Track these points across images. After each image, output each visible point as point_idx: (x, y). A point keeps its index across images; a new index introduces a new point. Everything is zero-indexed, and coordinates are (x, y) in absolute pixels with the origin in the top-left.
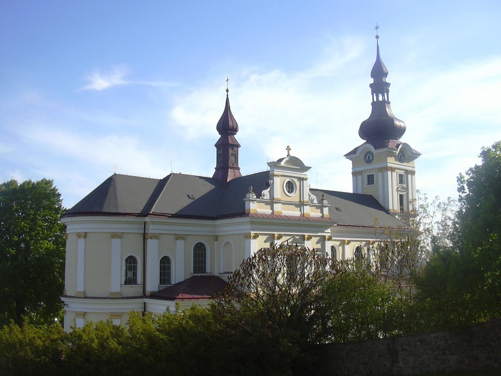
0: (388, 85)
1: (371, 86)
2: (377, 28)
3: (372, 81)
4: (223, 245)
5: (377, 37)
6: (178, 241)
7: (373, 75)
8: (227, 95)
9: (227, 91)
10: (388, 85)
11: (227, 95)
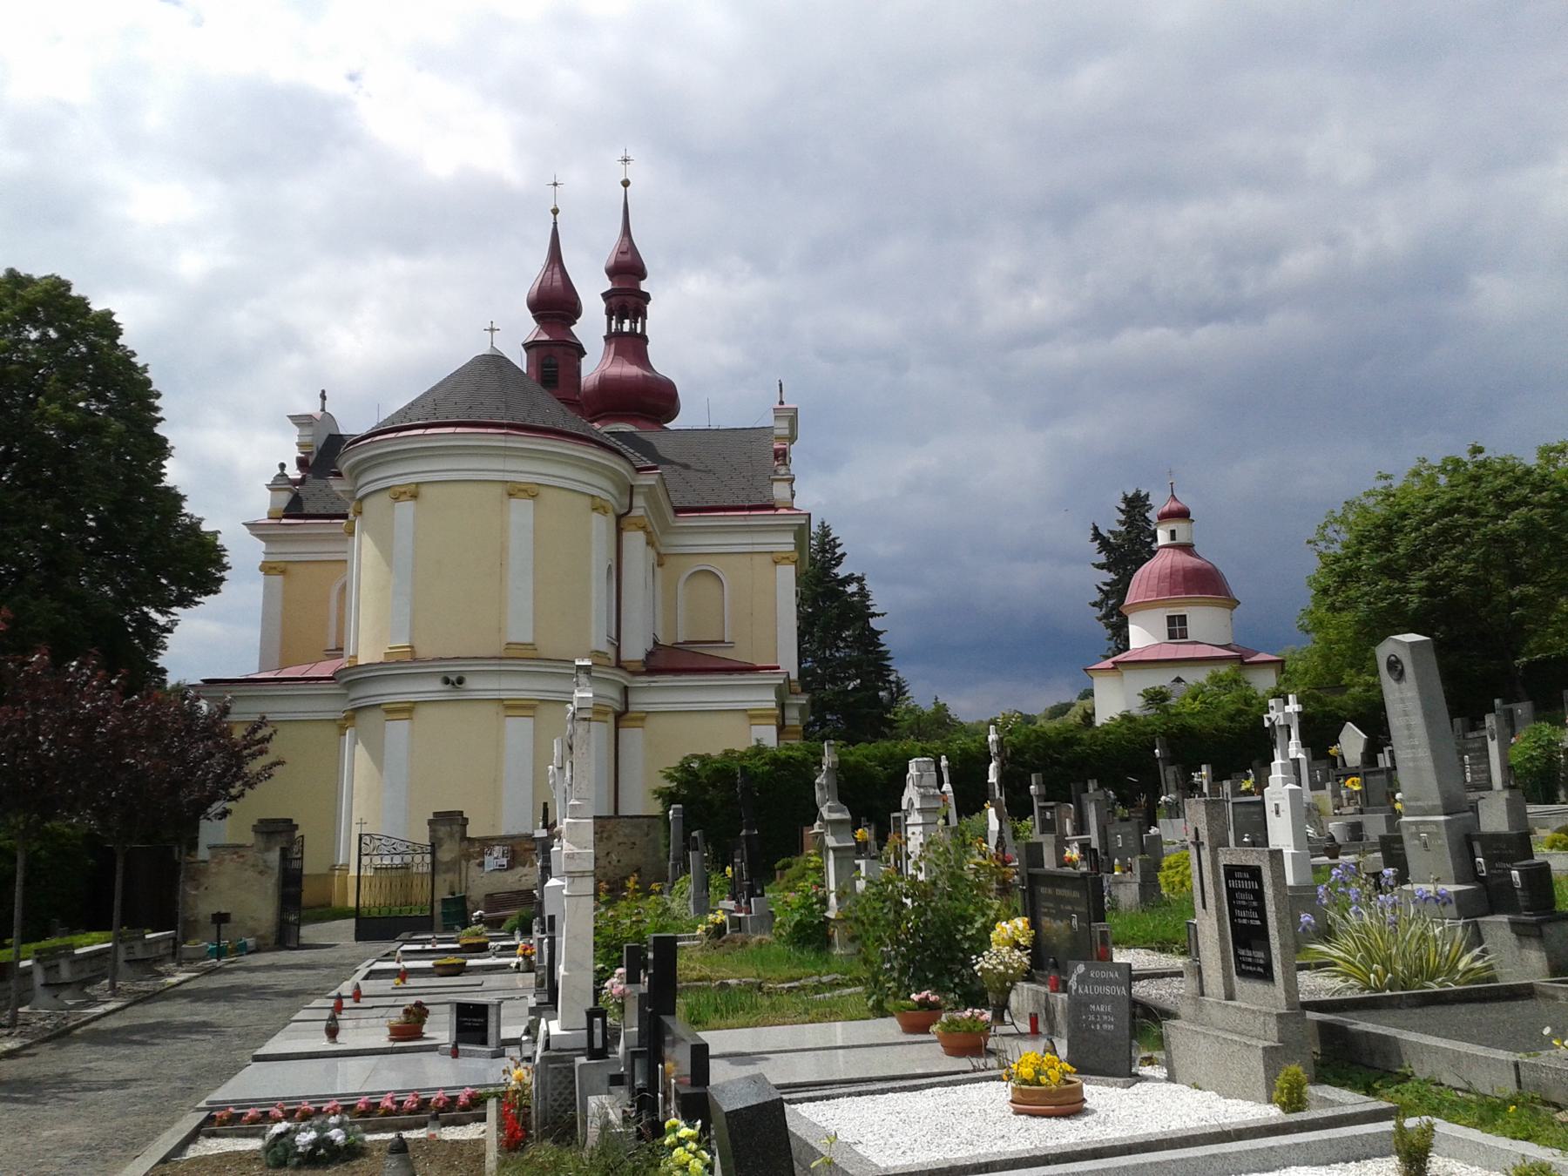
1: (606, 296)
2: (626, 160)
3: (644, 286)
4: (687, 575)
5: (626, 184)
6: (595, 514)
7: (613, 272)
8: (555, 224)
9: (555, 212)
11: (555, 224)
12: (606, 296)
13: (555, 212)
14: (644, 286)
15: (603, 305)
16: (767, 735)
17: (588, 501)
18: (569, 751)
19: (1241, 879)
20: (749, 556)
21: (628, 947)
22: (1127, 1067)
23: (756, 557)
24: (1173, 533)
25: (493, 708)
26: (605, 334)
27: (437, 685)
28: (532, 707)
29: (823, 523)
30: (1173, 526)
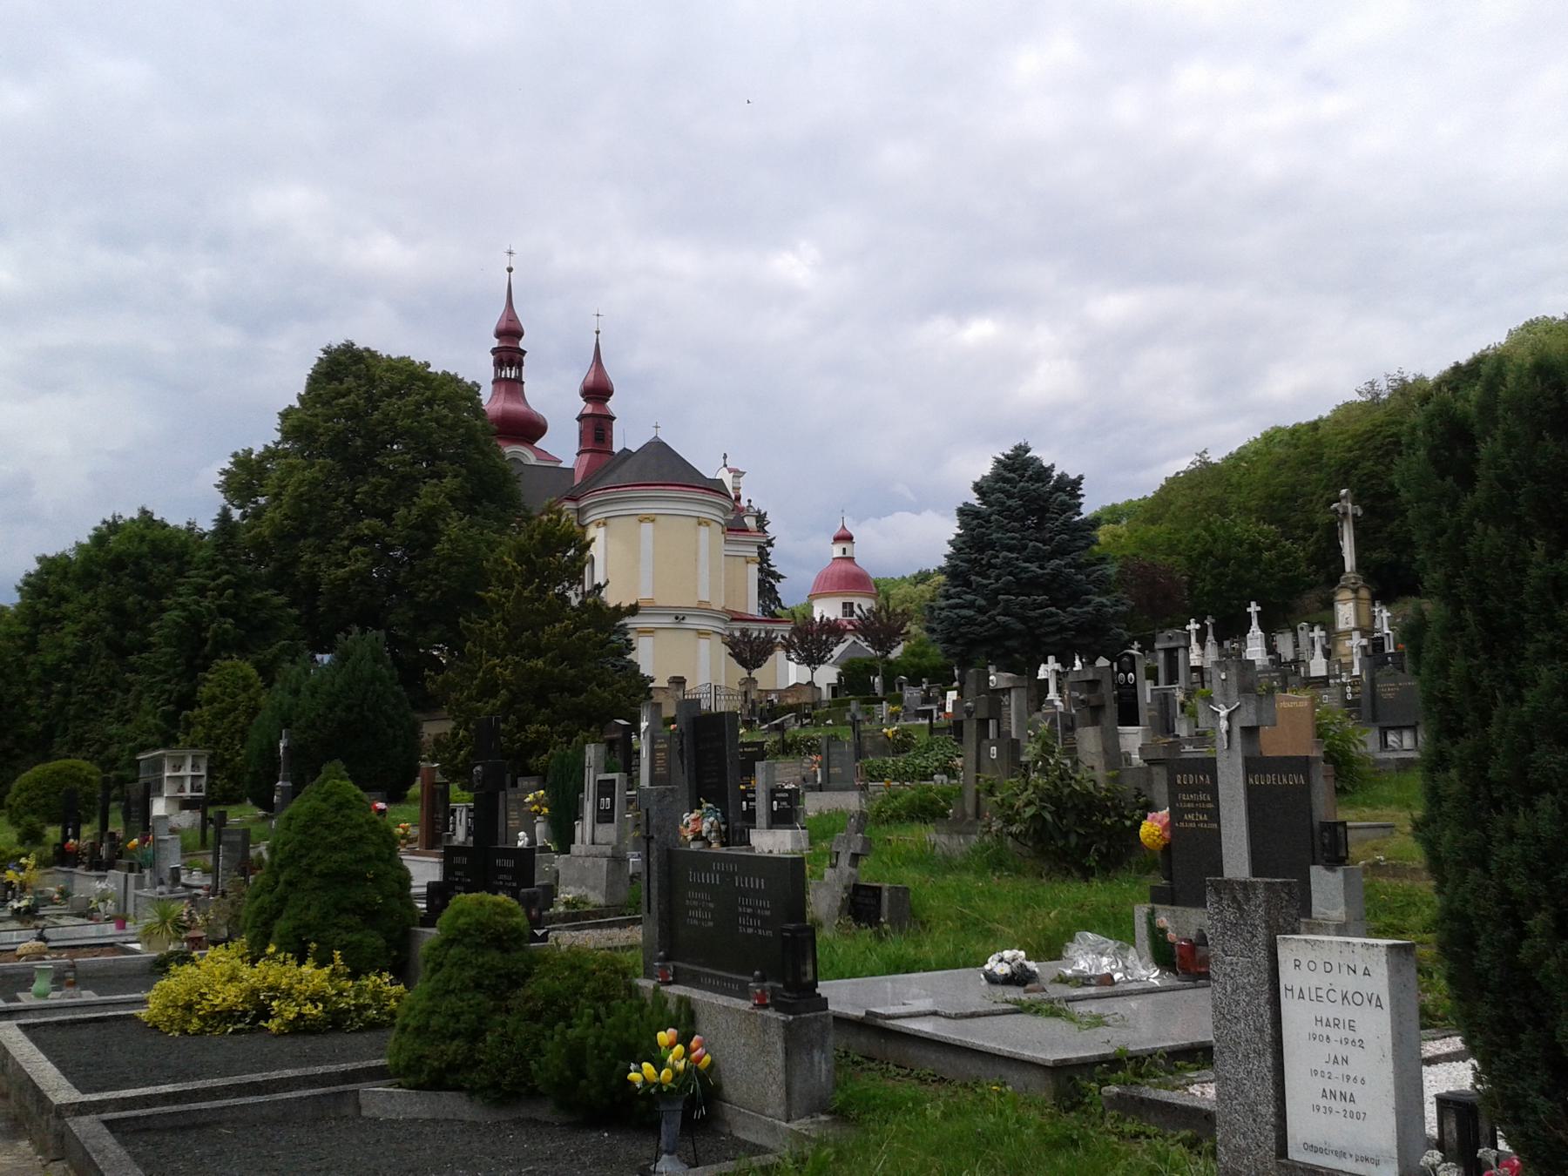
0: (523, 353)
1: (494, 351)
5: (510, 270)
8: (597, 345)
9: (598, 332)
10: (523, 353)
12: (494, 351)
13: (598, 332)
14: (522, 344)
15: (492, 358)
16: (942, 660)
17: (695, 520)
18: (1309, 647)
19: (694, 899)
20: (732, 558)
21: (614, 781)
22: (1392, 724)
23: (738, 559)
24: (844, 549)
25: (694, 633)
26: (492, 378)
27: (672, 619)
28: (652, 632)
29: (783, 577)
30: (844, 546)
